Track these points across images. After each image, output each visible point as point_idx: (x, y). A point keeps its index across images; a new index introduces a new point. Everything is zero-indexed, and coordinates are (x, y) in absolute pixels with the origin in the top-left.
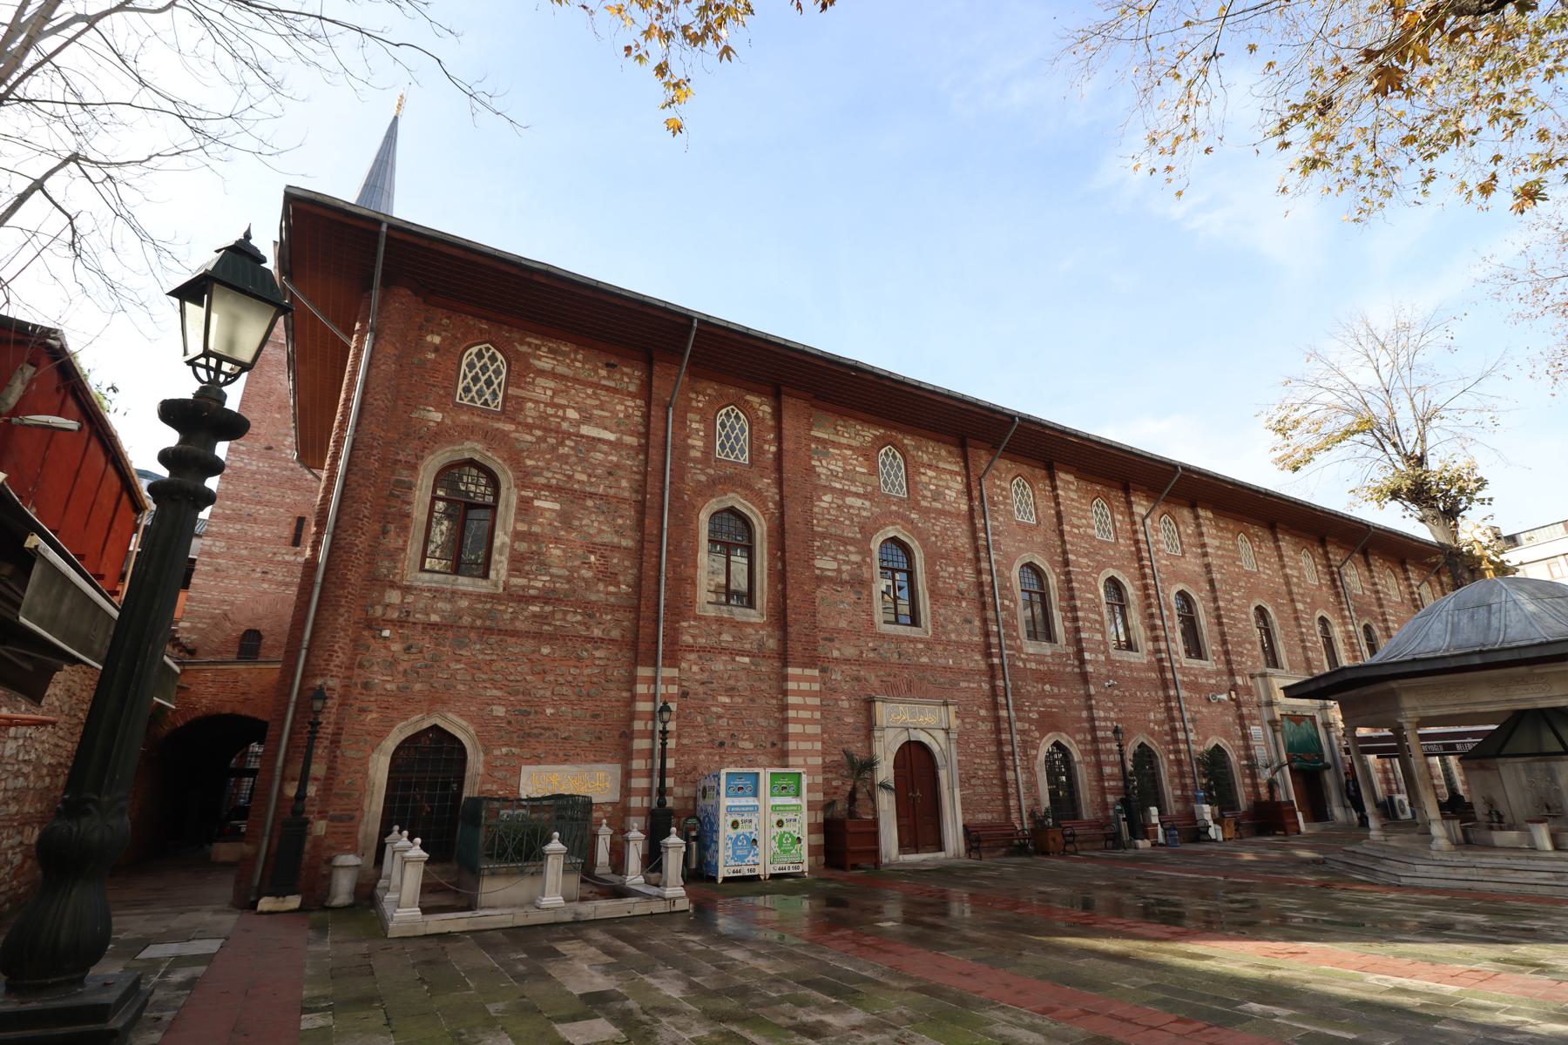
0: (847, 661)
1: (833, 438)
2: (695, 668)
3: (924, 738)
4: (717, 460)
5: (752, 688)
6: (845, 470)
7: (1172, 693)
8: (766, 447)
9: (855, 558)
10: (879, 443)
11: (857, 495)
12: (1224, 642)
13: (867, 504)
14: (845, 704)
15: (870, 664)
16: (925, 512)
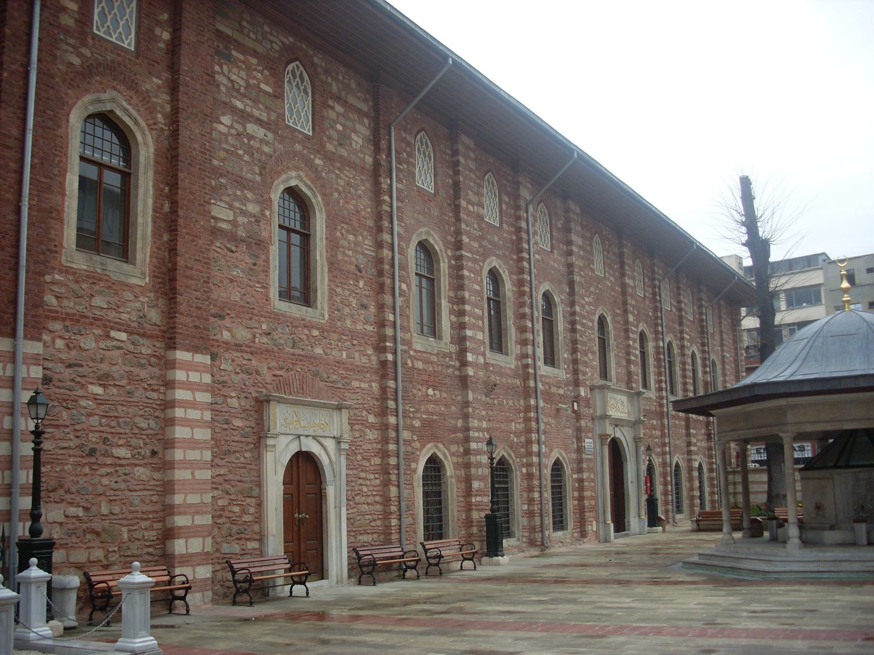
0: (238, 347)
1: (237, 36)
2: (60, 343)
3: (315, 448)
4: (95, 37)
5: (131, 378)
6: (248, 86)
7: (533, 402)
8: (158, 31)
9: (253, 208)
10: (290, 55)
11: (259, 122)
12: (574, 351)
13: (270, 136)
14: (234, 402)
15: (264, 353)
16: (329, 158)
